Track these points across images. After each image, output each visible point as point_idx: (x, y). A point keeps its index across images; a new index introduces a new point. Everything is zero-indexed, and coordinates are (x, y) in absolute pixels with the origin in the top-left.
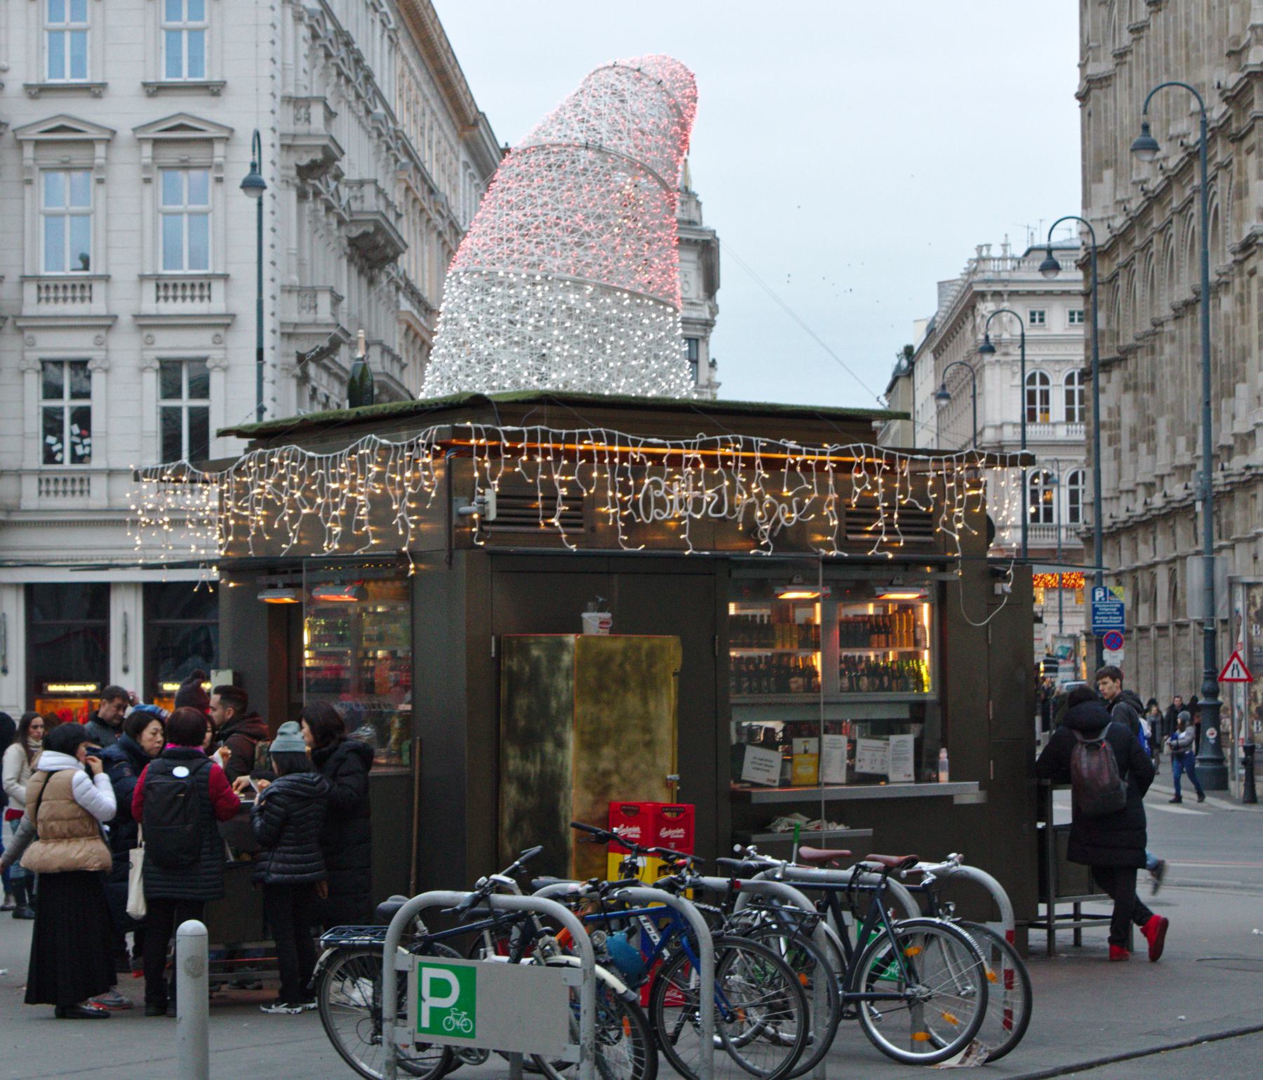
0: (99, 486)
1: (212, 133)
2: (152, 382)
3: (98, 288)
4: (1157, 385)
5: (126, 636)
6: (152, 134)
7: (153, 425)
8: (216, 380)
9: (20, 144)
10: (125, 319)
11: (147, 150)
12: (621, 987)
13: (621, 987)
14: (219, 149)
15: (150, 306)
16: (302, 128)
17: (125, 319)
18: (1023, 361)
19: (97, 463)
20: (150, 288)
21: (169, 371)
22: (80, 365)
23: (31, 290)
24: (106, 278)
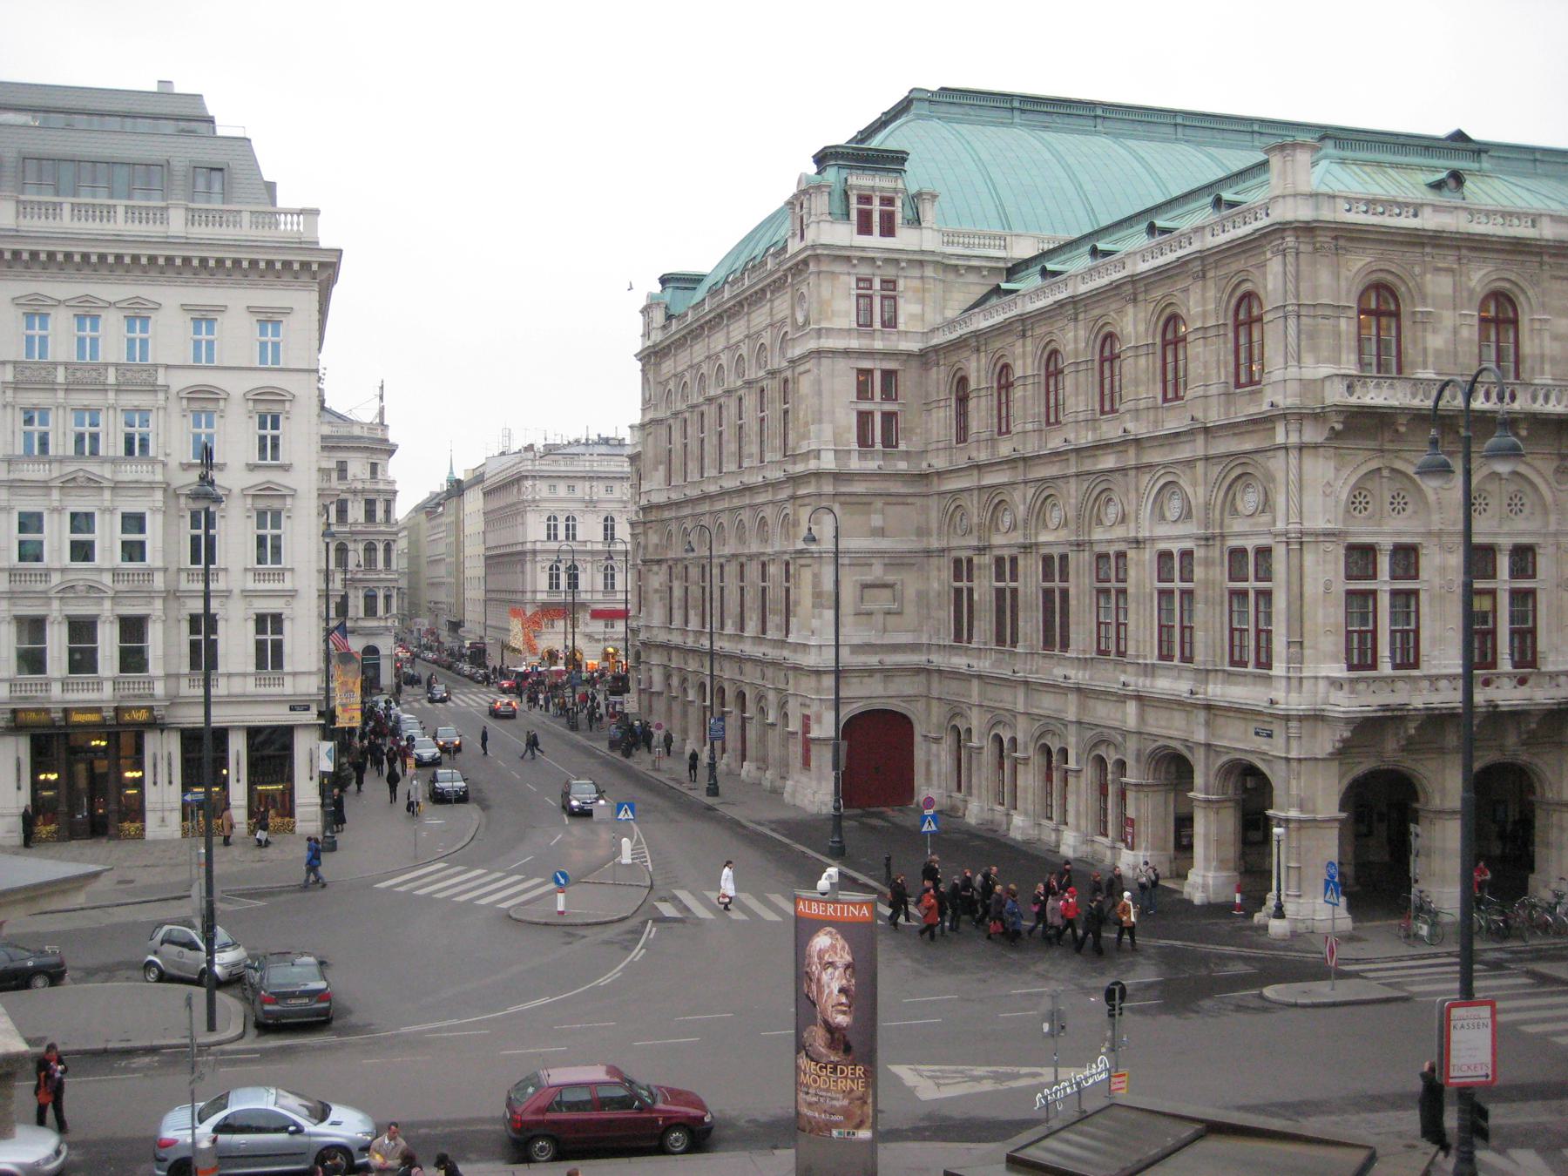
0: (288, 680)
1: (285, 492)
2: (251, 626)
3: (288, 575)
4: (449, 673)
5: (155, 766)
6: (252, 492)
7: (252, 649)
8: (287, 626)
9: (178, 496)
10: (236, 591)
11: (249, 501)
12: (404, 1030)
13: (404, 1030)
14: (289, 501)
15: (250, 585)
16: (325, 485)
17: (236, 591)
18: (837, 646)
19: (287, 668)
20: (250, 576)
21: (261, 620)
22: (277, 619)
23: (184, 576)
24: (226, 570)
